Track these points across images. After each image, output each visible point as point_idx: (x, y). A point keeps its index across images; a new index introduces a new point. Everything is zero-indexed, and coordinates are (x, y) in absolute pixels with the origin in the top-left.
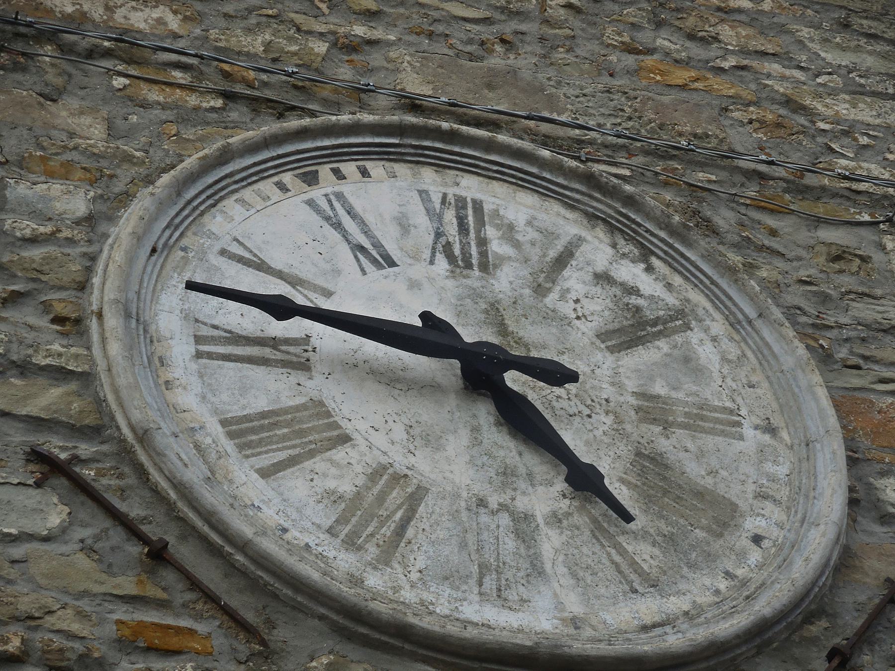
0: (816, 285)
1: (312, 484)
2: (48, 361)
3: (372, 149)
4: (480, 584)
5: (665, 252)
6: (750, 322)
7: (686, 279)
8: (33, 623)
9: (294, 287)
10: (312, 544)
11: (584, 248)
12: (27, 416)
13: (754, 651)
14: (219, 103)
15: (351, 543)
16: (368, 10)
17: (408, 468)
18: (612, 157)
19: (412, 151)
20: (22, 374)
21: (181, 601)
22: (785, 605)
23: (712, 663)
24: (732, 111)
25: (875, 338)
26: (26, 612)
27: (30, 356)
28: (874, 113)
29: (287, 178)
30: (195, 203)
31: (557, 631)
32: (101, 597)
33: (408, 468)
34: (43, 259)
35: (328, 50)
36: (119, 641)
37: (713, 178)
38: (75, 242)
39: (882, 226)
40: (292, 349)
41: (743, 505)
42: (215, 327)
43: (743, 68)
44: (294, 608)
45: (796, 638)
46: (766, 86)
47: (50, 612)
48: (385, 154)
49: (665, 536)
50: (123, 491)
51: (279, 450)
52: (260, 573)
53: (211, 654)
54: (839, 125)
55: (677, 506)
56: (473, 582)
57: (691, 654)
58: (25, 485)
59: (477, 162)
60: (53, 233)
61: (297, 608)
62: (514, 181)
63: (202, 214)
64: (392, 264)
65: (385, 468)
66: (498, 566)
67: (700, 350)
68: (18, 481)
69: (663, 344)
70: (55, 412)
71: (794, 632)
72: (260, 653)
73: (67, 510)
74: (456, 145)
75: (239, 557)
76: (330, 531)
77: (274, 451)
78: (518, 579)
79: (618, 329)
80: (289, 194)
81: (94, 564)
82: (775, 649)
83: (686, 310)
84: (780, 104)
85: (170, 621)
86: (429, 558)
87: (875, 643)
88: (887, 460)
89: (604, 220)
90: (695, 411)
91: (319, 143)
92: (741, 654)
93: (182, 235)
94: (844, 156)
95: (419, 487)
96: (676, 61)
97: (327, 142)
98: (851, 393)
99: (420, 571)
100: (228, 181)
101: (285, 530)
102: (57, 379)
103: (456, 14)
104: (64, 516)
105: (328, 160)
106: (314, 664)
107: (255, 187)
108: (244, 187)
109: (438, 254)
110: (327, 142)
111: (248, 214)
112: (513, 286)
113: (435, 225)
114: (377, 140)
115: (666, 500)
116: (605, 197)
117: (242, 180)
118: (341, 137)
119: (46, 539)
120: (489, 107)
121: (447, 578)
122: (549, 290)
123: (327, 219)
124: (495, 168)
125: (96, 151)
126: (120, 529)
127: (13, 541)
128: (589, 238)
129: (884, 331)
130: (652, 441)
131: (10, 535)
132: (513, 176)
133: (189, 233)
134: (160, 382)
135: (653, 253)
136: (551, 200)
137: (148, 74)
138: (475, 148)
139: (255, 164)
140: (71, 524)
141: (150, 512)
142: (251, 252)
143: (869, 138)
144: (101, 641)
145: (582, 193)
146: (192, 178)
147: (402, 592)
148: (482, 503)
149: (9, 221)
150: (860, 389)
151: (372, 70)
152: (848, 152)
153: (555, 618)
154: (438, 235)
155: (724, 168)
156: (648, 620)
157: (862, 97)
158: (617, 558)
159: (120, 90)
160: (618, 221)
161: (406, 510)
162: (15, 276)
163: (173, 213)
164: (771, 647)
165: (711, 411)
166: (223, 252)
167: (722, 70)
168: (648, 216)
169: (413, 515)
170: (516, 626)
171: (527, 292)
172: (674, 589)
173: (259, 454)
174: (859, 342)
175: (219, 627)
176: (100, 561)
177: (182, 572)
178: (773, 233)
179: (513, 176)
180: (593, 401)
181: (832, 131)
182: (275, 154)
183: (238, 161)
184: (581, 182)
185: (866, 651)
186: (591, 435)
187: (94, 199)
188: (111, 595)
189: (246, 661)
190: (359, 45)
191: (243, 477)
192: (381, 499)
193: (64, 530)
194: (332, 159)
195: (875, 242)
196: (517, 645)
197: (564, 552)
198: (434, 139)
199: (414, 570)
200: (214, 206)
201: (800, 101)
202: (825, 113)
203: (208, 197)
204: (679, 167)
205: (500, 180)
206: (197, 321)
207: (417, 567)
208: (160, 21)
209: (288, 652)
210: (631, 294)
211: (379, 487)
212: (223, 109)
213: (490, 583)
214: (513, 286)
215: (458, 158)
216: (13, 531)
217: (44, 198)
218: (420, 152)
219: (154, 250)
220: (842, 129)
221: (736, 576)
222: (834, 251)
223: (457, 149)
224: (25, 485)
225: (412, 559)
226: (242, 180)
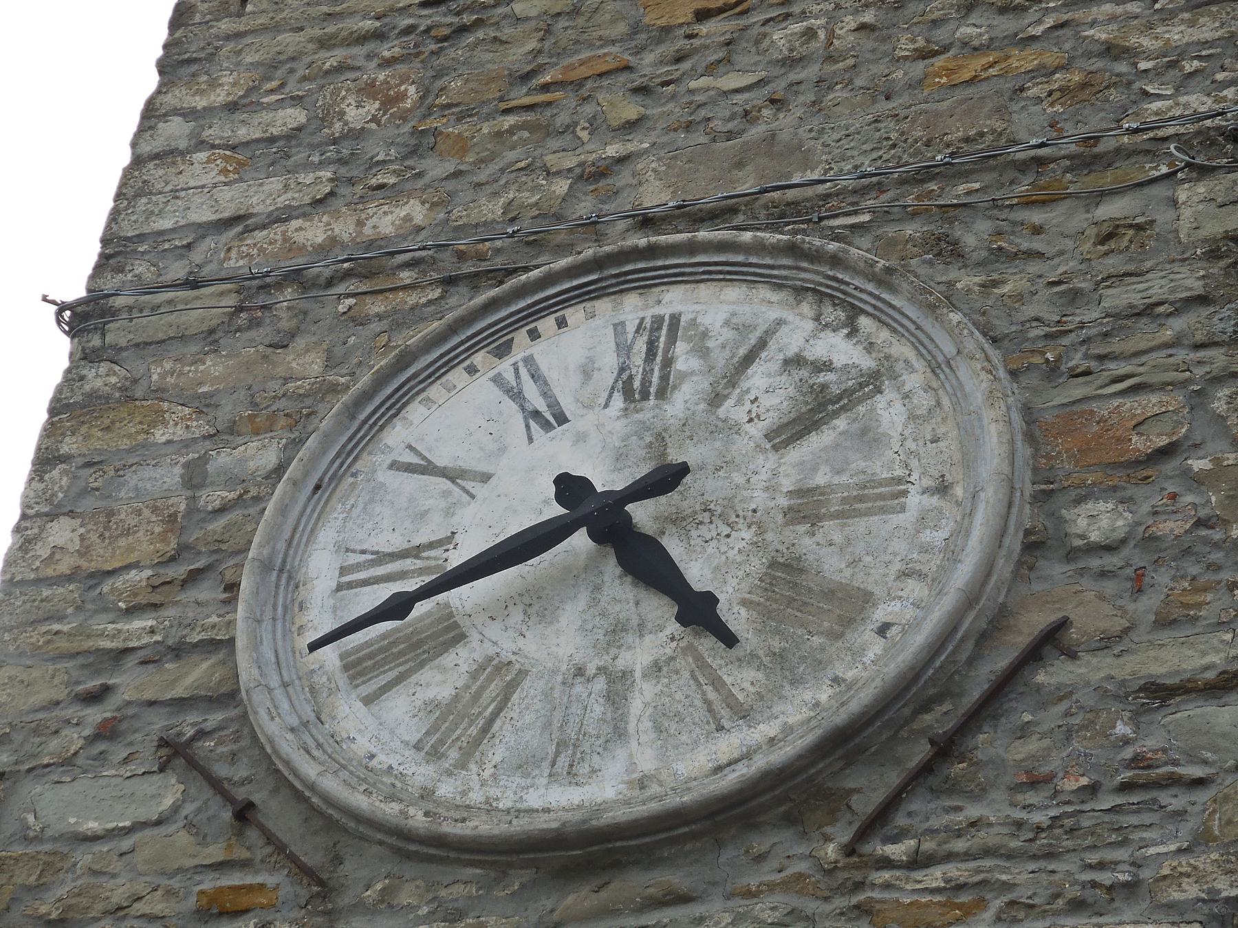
0: (1066, 283)
1: (413, 698)
2: (203, 636)
3: (572, 294)
4: (553, 764)
5: (875, 307)
6: (281, 571)
7: (895, 331)
8: (121, 913)
9: (453, 482)
10: (395, 766)
11: (784, 329)
12: (171, 699)
13: (841, 764)
14: (438, 292)
15: (435, 754)
16: (628, 122)
17: (514, 653)
18: (856, 203)
19: (614, 281)
20: (177, 656)
21: (260, 857)
22: (866, 706)
23: (777, 792)
24: (1029, 89)
25: (1121, 328)
26: (117, 904)
27: (185, 636)
28: (1217, 24)
29: (479, 359)
30: (371, 422)
31: (621, 796)
32: (192, 871)
33: (514, 653)
34: (223, 528)
35: (570, 187)
36: (198, 911)
37: (977, 186)
38: (261, 498)
39: (1179, 175)
40: (432, 553)
41: (878, 591)
42: (363, 552)
43: (1062, 25)
44: (361, 838)
45: (904, 734)
46: (1087, 37)
47: (139, 899)
48: (585, 295)
49: (775, 654)
50: (234, 755)
51: (391, 669)
52: (330, 811)
53: (274, 906)
54: (1165, 57)
55: (799, 614)
56: (546, 765)
57: (740, 791)
58: (149, 773)
59: (682, 270)
60: (241, 496)
61: (362, 838)
62: (721, 277)
63: (382, 428)
64: (562, 419)
65: (491, 659)
66: (578, 739)
67: (885, 414)
68: (143, 770)
69: (841, 423)
70: (196, 688)
71: (902, 727)
72: (318, 893)
73: (182, 787)
74: (659, 258)
75: (315, 800)
76: (417, 747)
77: (384, 672)
78: (595, 748)
79: (794, 419)
80: (478, 374)
81: (192, 838)
82: (873, 754)
83: (882, 369)
84: (1100, 55)
85: (249, 880)
86: (507, 749)
87: (1002, 715)
88: (1089, 482)
89: (814, 290)
90: (855, 493)
91: (513, 308)
92: (820, 772)
93: (356, 459)
94: (1159, 97)
95: (520, 671)
96: (975, 49)
97: (522, 304)
98: (1068, 410)
99: (495, 767)
100: (412, 383)
101: (372, 756)
102: (210, 652)
103: (725, 89)
104: (179, 795)
105: (525, 322)
106: (369, 893)
107: (444, 379)
108: (431, 384)
109: (616, 393)
110: (522, 304)
111: (430, 412)
112: (688, 405)
113: (621, 360)
114: (575, 283)
115: (789, 610)
116: (812, 264)
117: (429, 376)
118: (537, 292)
119: (158, 823)
120: (720, 195)
121: (520, 767)
122: (726, 397)
123: (508, 391)
124: (702, 269)
125: (301, 391)
126: (218, 797)
127: (127, 833)
128: (790, 318)
129: (1138, 314)
130: (793, 545)
131: (124, 828)
132: (720, 272)
133: (365, 455)
134: (293, 629)
135: (863, 311)
136: (760, 286)
137: (377, 285)
138: (679, 254)
139: (442, 356)
140: (184, 801)
141: (253, 771)
142: (421, 455)
143: (1200, 61)
144: (180, 916)
145: (789, 268)
146: (366, 396)
147: (470, 794)
148: (580, 671)
149: (204, 497)
150: (1079, 401)
151: (618, 192)
152: (1166, 89)
153: (623, 782)
154: (622, 370)
155: (993, 169)
156: (724, 759)
157: (1208, 7)
158: (712, 695)
159: (345, 313)
160: (828, 287)
161: (500, 702)
162: (200, 553)
163: (344, 439)
164: (868, 753)
165: (873, 488)
166: (395, 466)
167: (1033, 38)
168: (856, 271)
169: (506, 705)
170: (577, 803)
171: (703, 406)
172: (768, 713)
173: (370, 679)
174: (1100, 338)
175: (287, 875)
176: (197, 834)
177: (929, 660)
178: (1037, 230)
179: (720, 272)
180: (738, 516)
181: (1155, 68)
182: (463, 337)
183: (422, 359)
184: (787, 256)
185: (986, 728)
186: (724, 557)
187: (285, 447)
188: (202, 866)
189: (306, 905)
190: (607, 168)
191: (347, 710)
192: (476, 697)
193: (176, 809)
194: (530, 319)
195: (1168, 198)
196: (543, 830)
197: (654, 704)
198: (636, 261)
199: (489, 766)
200: (395, 415)
201: (1123, 44)
202: (1152, 48)
203: (388, 409)
204: (936, 188)
205: (708, 280)
206: (347, 550)
207: (493, 763)
208: (408, 219)
209: (348, 886)
210: (820, 371)
211: (478, 683)
212: (441, 298)
213: (563, 761)
214: (688, 405)
215: (662, 272)
216: (127, 824)
217: (242, 461)
218: (623, 279)
219: (317, 487)
220: (1168, 62)
221: (844, 680)
222: (1105, 229)
223: (660, 263)
224: (149, 773)
225: (491, 753)
226: (429, 376)
